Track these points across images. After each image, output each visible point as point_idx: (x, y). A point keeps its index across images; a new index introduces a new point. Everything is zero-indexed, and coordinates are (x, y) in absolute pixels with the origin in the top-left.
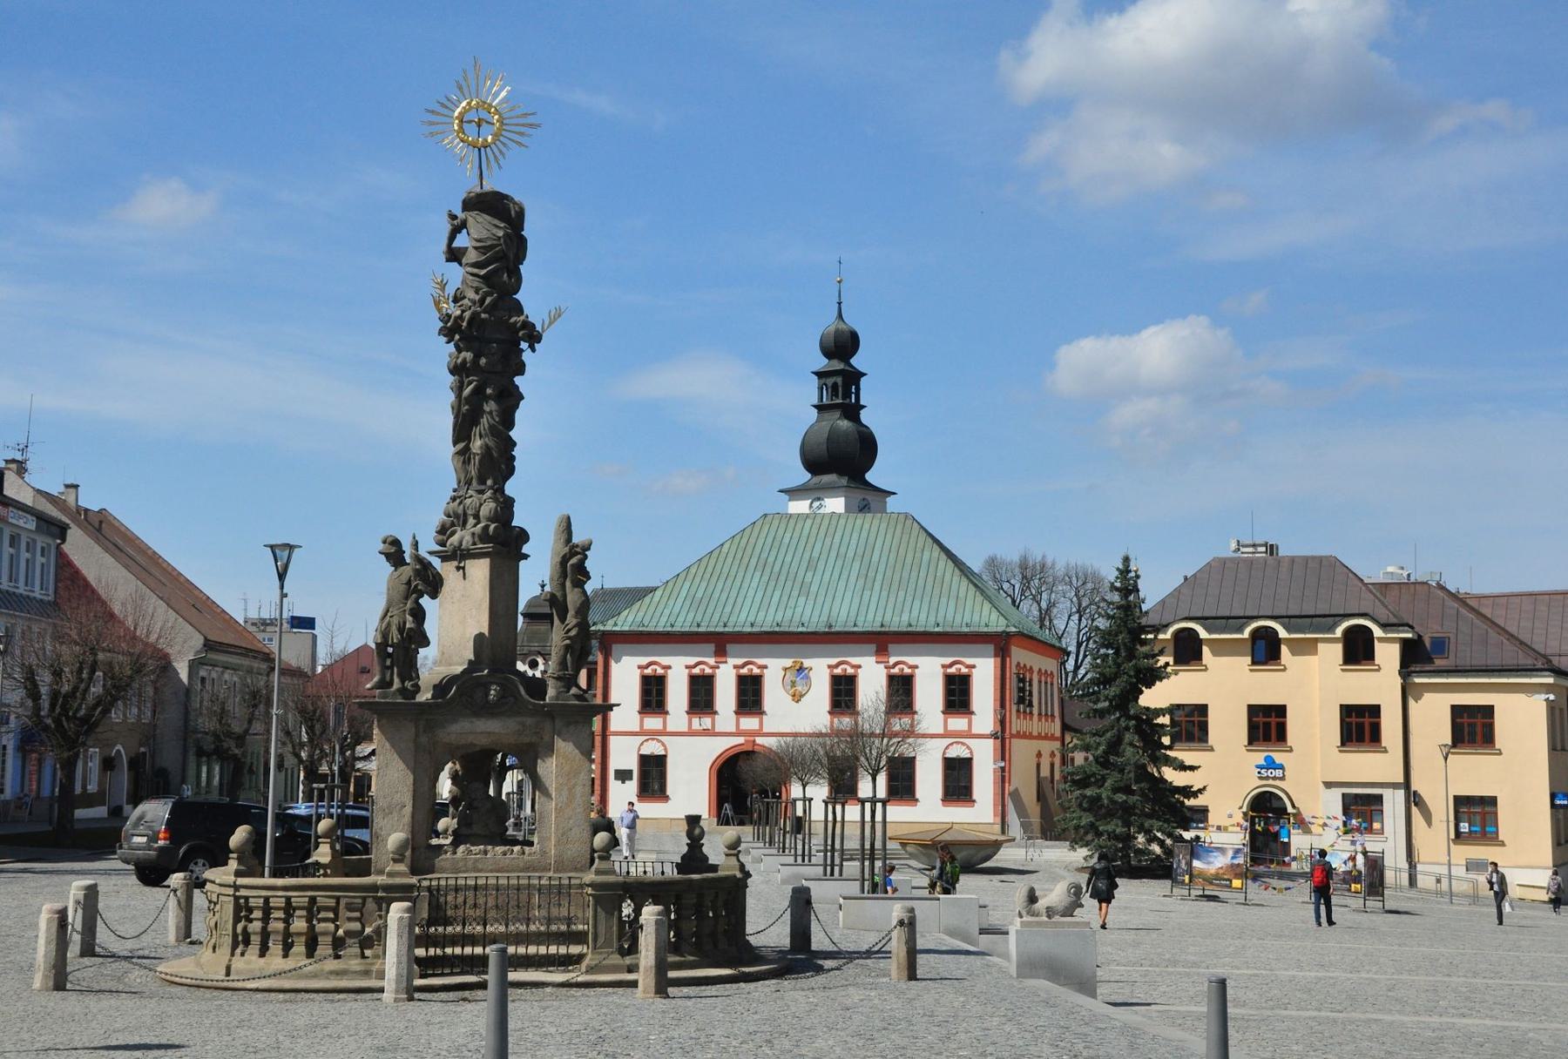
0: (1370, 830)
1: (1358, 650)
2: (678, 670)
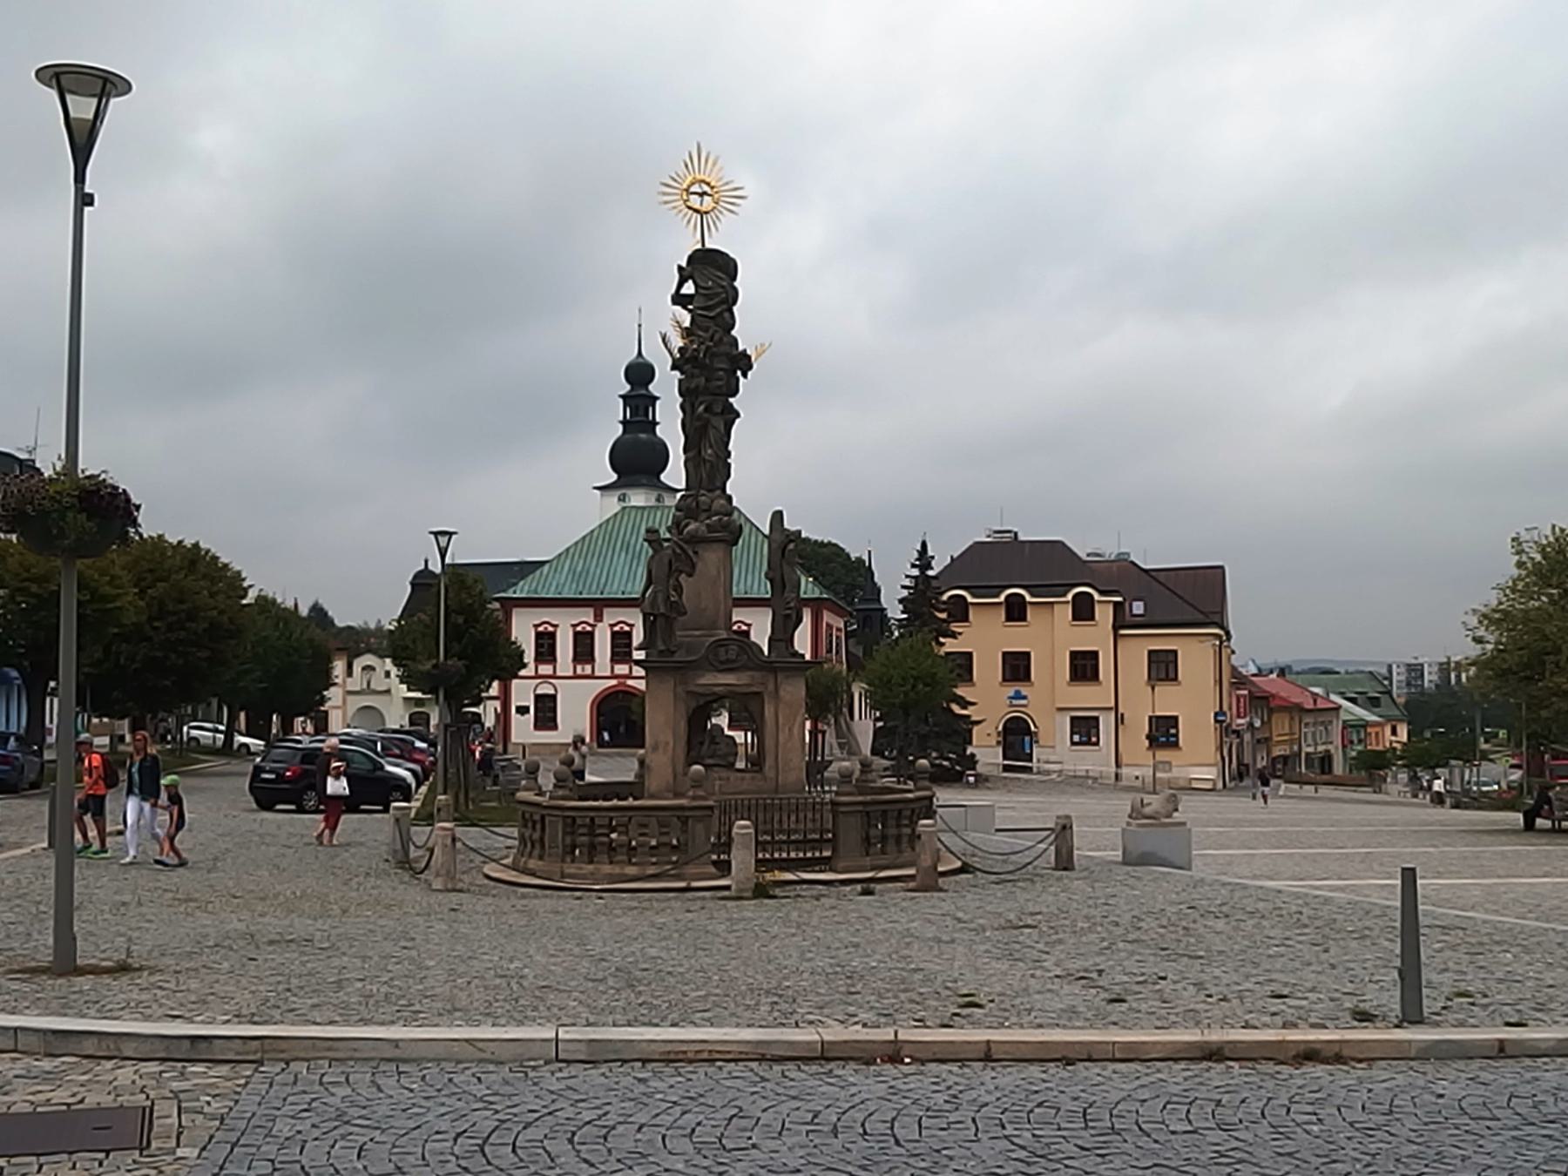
0: (1089, 743)
1: (1083, 611)
2: (565, 625)
